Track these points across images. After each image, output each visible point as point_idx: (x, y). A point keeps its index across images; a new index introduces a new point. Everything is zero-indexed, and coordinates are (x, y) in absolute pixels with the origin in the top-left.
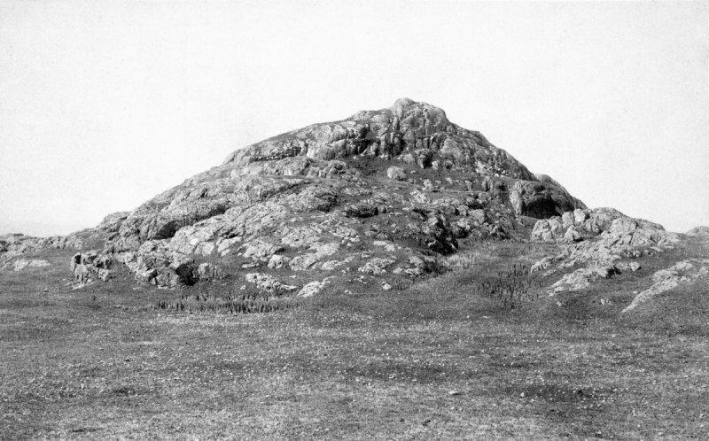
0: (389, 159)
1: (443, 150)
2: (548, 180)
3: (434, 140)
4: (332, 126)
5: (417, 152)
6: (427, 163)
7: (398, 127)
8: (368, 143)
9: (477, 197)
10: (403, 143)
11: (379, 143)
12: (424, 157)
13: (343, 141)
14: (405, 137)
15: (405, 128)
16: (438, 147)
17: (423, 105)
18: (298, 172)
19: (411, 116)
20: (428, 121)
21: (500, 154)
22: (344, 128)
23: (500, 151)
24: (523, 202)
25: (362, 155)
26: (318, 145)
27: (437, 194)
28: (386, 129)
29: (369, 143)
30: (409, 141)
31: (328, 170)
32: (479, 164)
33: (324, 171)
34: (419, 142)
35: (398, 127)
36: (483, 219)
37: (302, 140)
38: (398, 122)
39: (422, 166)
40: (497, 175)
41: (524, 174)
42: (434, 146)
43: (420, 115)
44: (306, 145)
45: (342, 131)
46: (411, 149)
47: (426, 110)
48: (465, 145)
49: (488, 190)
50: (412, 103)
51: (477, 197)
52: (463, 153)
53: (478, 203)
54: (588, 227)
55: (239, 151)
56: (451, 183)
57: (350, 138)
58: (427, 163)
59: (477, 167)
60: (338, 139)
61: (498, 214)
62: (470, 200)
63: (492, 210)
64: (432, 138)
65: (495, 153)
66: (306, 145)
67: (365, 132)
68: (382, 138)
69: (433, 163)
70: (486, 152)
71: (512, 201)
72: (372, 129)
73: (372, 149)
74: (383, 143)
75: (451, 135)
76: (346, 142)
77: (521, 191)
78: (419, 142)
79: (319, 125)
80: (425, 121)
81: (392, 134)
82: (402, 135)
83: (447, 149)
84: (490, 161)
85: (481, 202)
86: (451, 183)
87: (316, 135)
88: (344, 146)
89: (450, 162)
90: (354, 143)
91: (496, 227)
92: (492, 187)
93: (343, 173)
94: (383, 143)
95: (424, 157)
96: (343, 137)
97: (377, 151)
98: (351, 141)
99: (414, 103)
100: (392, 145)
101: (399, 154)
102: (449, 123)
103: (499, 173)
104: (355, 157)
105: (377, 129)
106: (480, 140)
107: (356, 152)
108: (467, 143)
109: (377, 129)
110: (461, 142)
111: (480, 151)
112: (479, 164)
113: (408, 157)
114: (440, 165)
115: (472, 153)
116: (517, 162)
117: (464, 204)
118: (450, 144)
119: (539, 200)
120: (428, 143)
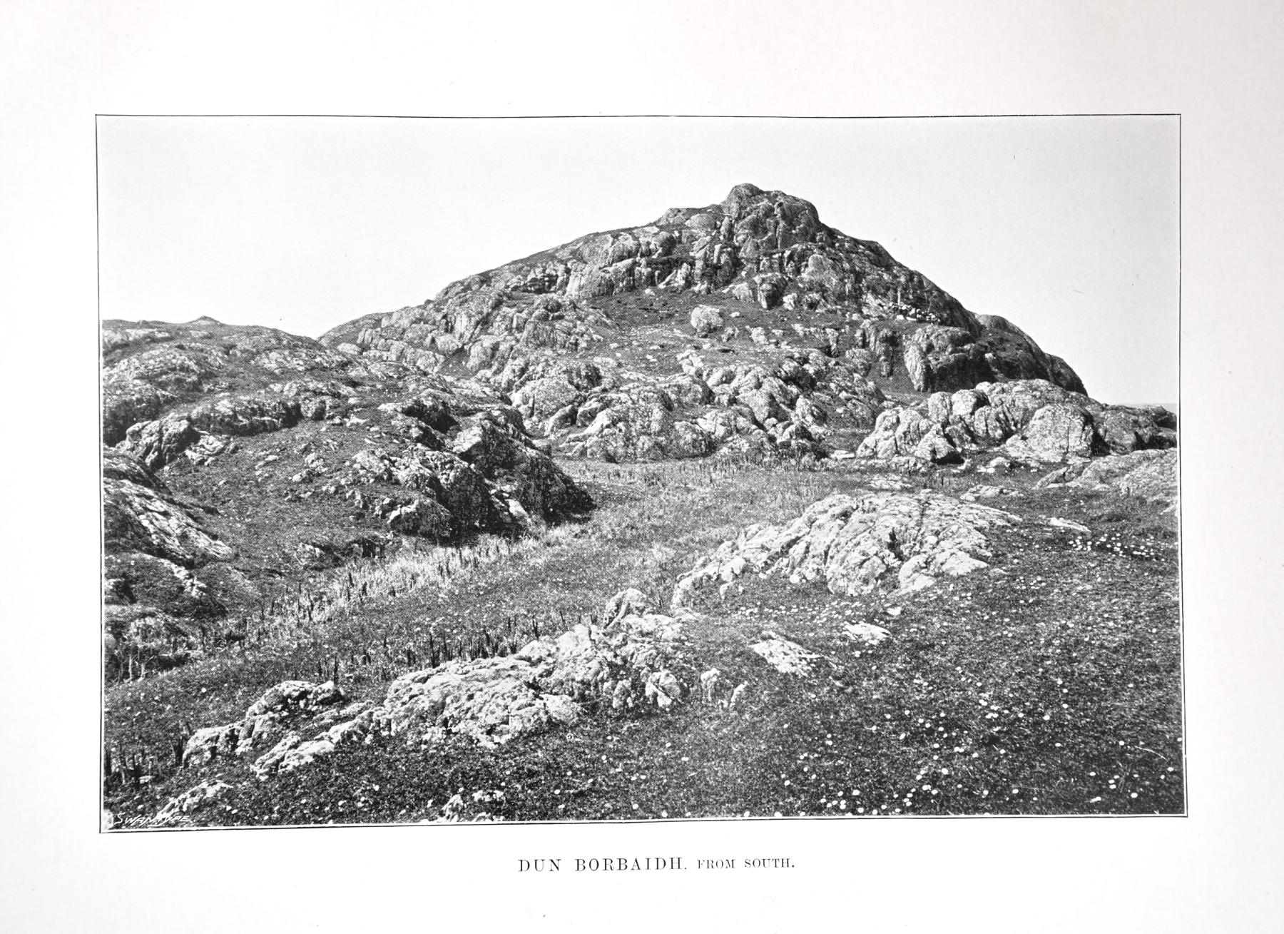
0: (709, 291)
1: (805, 275)
2: (1001, 324)
3: (791, 257)
4: (616, 235)
5: (757, 279)
6: (775, 299)
7: (731, 233)
8: (668, 266)
9: (805, 360)
10: (736, 264)
11: (692, 265)
12: (769, 287)
13: (629, 261)
14: (741, 254)
15: (741, 238)
16: (798, 271)
17: (776, 196)
18: (477, 318)
19: (753, 215)
20: (782, 224)
21: (911, 280)
22: (636, 239)
23: (911, 275)
24: (928, 368)
25: (662, 286)
26: (587, 269)
27: (726, 357)
28: (708, 238)
29: (678, 263)
30: (747, 260)
31: (530, 314)
32: (869, 298)
33: (524, 315)
34: (764, 260)
35: (731, 233)
36: (765, 410)
37: (561, 261)
38: (731, 226)
39: (764, 304)
40: (900, 317)
41: (951, 311)
42: (789, 268)
43: (769, 212)
44: (568, 271)
45: (630, 243)
46: (749, 275)
47: (781, 205)
48: (847, 266)
49: (865, 345)
50: (755, 192)
51: (805, 360)
52: (841, 280)
53: (805, 372)
54: (980, 427)
55: (454, 285)
56: (801, 334)
57: (642, 256)
58: (775, 299)
59: (865, 304)
60: (621, 258)
61: (843, 395)
62: (788, 367)
63: (832, 385)
64: (787, 253)
65: (903, 279)
66: (568, 271)
67: (670, 244)
68: (700, 254)
69: (785, 299)
70: (886, 276)
71: (908, 365)
72: (684, 240)
73: (678, 277)
74: (699, 264)
75: (822, 248)
76: (635, 264)
77: (924, 346)
78: (764, 260)
79: (597, 234)
80: (777, 223)
81: (717, 247)
82: (737, 249)
83: (812, 273)
84: (890, 293)
85: (811, 371)
86: (801, 334)
87: (586, 253)
88: (630, 271)
89: (816, 296)
90: (649, 264)
91: (792, 428)
92: (872, 339)
93: (561, 317)
94: (699, 264)
95: (769, 287)
96: (630, 254)
97: (689, 282)
98: (643, 261)
99: (761, 192)
100: (717, 267)
101: (727, 283)
102: (823, 227)
103: (905, 313)
104: (648, 291)
105: (693, 238)
106: (879, 256)
107: (651, 281)
108: (850, 261)
109: (693, 238)
110: (840, 260)
111: (873, 275)
112: (869, 298)
113: (740, 289)
114: (798, 302)
115: (859, 276)
116: (941, 293)
117: (775, 375)
118: (819, 265)
119: (957, 361)
120: (781, 265)
